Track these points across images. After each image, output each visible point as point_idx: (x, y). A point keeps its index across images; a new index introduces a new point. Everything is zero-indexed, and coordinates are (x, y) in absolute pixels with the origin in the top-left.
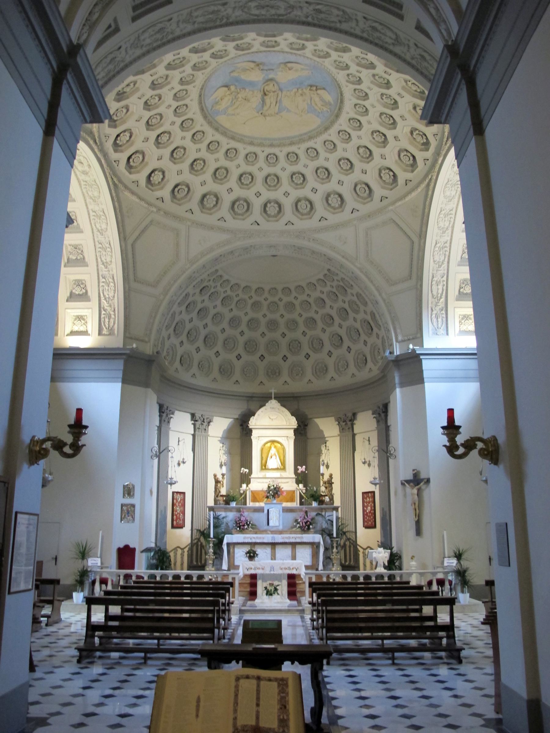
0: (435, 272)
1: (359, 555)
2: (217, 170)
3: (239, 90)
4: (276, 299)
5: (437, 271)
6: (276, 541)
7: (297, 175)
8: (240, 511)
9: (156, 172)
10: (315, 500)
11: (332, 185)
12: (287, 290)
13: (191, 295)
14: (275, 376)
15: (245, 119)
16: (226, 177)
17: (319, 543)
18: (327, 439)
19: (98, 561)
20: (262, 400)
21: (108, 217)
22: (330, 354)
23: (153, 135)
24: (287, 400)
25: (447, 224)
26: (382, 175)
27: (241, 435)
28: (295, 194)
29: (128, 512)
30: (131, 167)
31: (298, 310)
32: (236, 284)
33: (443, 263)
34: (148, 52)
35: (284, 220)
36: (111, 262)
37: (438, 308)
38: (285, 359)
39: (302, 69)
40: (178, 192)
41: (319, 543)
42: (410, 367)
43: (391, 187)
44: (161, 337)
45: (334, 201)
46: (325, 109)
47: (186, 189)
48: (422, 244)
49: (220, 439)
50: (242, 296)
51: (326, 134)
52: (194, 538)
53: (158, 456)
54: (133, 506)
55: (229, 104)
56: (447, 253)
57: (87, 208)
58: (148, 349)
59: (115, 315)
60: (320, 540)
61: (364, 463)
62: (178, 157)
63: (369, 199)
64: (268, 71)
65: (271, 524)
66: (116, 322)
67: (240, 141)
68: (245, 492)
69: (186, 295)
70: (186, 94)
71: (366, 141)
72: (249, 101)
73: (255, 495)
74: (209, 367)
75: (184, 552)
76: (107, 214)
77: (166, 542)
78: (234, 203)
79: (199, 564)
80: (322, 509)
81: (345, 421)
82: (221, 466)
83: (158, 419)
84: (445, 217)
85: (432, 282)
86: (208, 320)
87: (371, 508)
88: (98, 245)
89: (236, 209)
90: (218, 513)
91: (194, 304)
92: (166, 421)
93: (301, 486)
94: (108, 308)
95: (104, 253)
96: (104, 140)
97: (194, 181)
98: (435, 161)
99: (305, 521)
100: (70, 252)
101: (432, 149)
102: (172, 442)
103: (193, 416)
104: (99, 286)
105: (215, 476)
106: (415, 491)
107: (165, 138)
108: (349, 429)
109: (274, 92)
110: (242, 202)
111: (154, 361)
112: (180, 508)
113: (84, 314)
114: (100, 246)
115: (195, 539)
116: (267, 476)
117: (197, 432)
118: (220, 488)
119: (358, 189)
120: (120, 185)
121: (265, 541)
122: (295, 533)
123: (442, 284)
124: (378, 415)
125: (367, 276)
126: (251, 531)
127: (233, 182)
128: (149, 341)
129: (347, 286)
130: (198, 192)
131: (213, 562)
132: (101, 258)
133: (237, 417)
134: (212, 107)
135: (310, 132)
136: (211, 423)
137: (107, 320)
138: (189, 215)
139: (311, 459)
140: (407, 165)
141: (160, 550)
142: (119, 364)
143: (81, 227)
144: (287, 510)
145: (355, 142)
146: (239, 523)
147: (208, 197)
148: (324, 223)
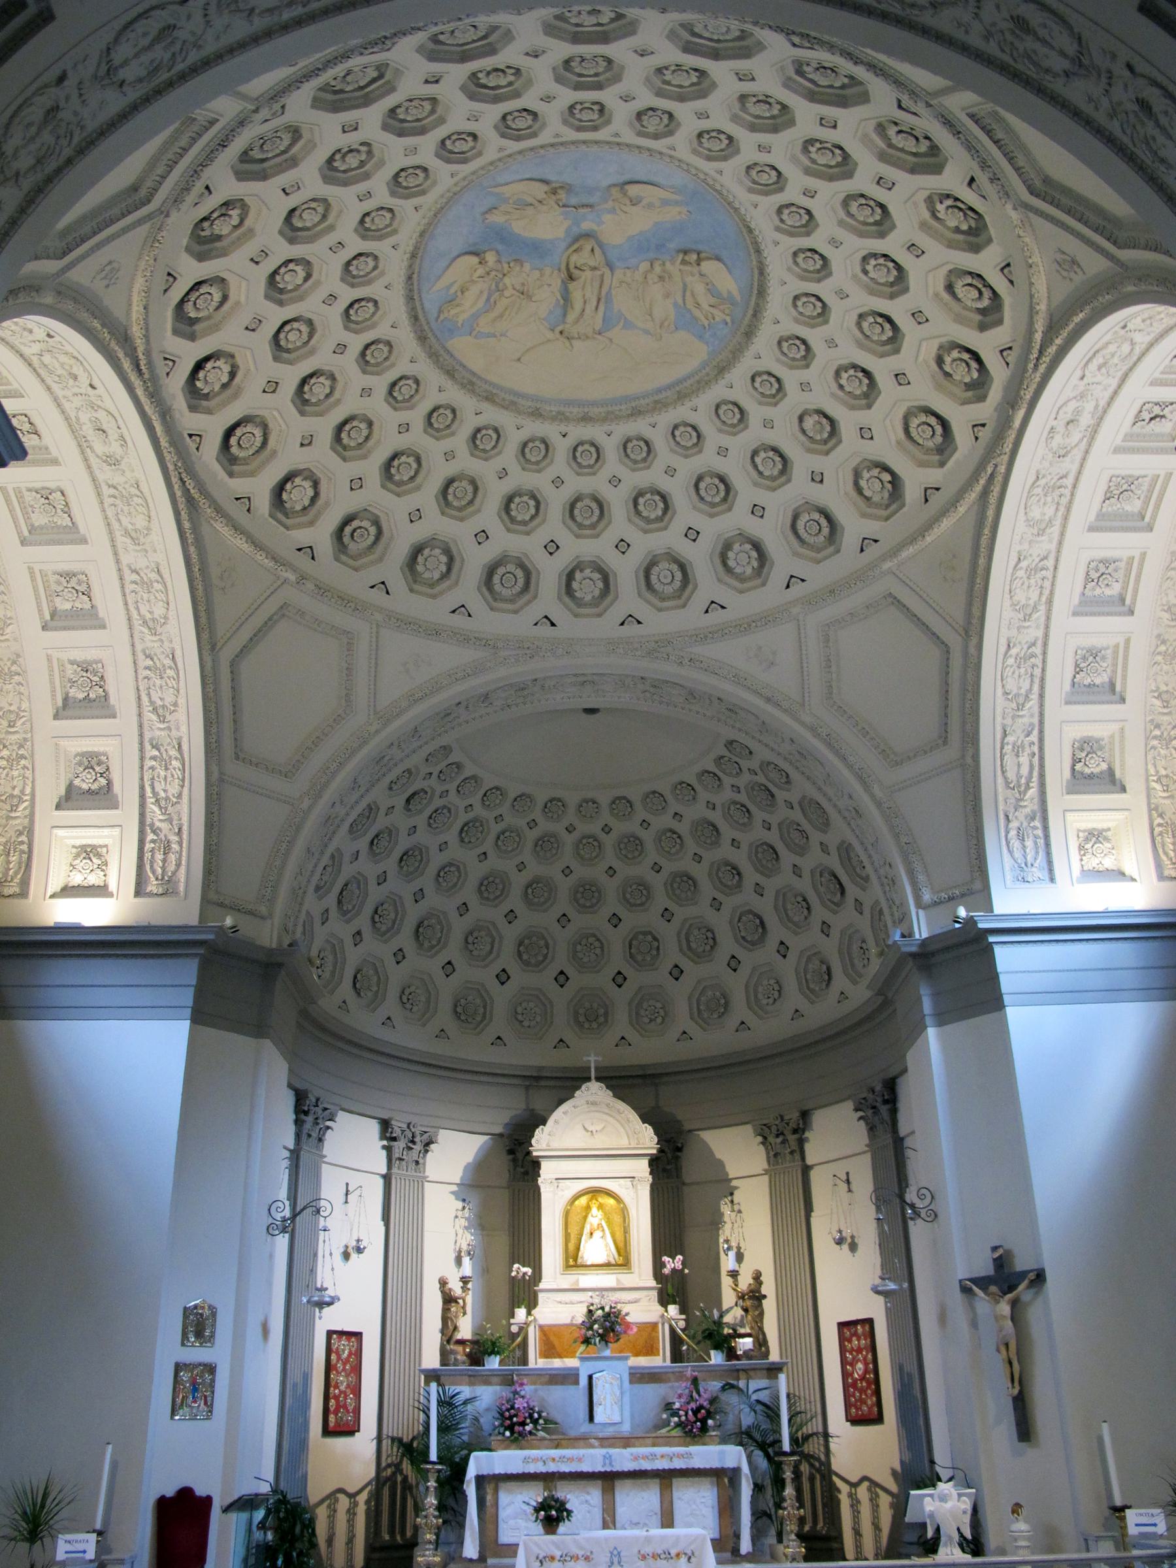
0: (1009, 721)
1: (839, 1502)
2: (450, 482)
3: (506, 266)
4: (595, 828)
5: (1013, 718)
6: (617, 1468)
7: (648, 496)
8: (511, 1383)
9: (298, 481)
10: (716, 1348)
11: (737, 519)
12: (622, 805)
13: (382, 812)
14: (595, 1025)
15: (522, 350)
16: (471, 502)
17: (736, 1471)
18: (734, 1183)
19: (88, 1544)
20: (564, 1084)
21: (169, 584)
22: (734, 963)
23: (290, 376)
24: (630, 1084)
25: (1034, 596)
26: (863, 483)
27: (511, 1175)
28: (645, 544)
29: (194, 1387)
30: (233, 460)
31: (652, 854)
32: (497, 788)
33: (1027, 696)
34: (269, 34)
35: (618, 611)
36: (175, 704)
37: (1022, 814)
38: (619, 979)
39: (665, 203)
40: (352, 536)
41: (736, 1471)
42: (962, 969)
43: (885, 513)
44: (304, 912)
45: (741, 557)
46: (719, 317)
47: (373, 530)
48: (972, 650)
49: (455, 1188)
50: (510, 820)
51: (722, 382)
52: (384, 1464)
53: (288, 1226)
54: (211, 1369)
55: (480, 304)
56: (1037, 672)
57: (118, 561)
58: (267, 935)
59: (180, 843)
60: (740, 1461)
61: (840, 1242)
62: (352, 444)
63: (831, 549)
64: (581, 210)
65: (598, 1418)
66: (184, 859)
67: (510, 406)
68: (523, 1328)
69: (369, 807)
70: (375, 268)
71: (823, 397)
72: (530, 297)
73: (552, 1338)
74: (428, 1001)
75: (356, 1504)
76: (166, 576)
77: (305, 1477)
78: (491, 571)
79: (398, 1538)
80: (738, 1370)
81: (782, 1134)
82: (459, 1261)
83: (292, 1129)
84: (1028, 578)
85: (1002, 748)
86: (426, 881)
87: (866, 1364)
88: (144, 662)
89: (497, 587)
90: (452, 1389)
91: (390, 835)
92: (315, 1135)
93: (673, 1310)
94: (164, 826)
95: (158, 682)
96: (161, 368)
97: (393, 508)
98: (1004, 423)
99: (693, 1405)
100: (70, 680)
101: (995, 393)
102: (331, 1186)
103: (385, 1125)
104: (142, 767)
105: (443, 1283)
106: (1005, 1308)
107: (319, 389)
108: (792, 1153)
109: (594, 269)
110: (511, 567)
111: (280, 965)
112: (347, 1376)
113: (101, 842)
114: (149, 662)
115: (389, 1466)
116: (582, 1285)
117: (394, 1170)
118: (456, 1317)
119: (800, 525)
120: (202, 502)
121: (586, 1468)
122: (668, 1441)
123: (1028, 751)
124: (870, 1112)
125: (829, 745)
126: (543, 1439)
127: (488, 515)
128: (271, 916)
129: (775, 785)
130: (403, 538)
131: (437, 1535)
132: (149, 695)
133: (498, 1129)
134: (440, 312)
135: (680, 382)
136: (432, 1146)
137: (159, 857)
138: (377, 596)
139: (693, 1238)
140: (928, 451)
141: (283, 1501)
142: (188, 971)
143: (101, 615)
144: (640, 1377)
145: (795, 400)
146: (511, 1418)
147: (426, 552)
148: (717, 616)
